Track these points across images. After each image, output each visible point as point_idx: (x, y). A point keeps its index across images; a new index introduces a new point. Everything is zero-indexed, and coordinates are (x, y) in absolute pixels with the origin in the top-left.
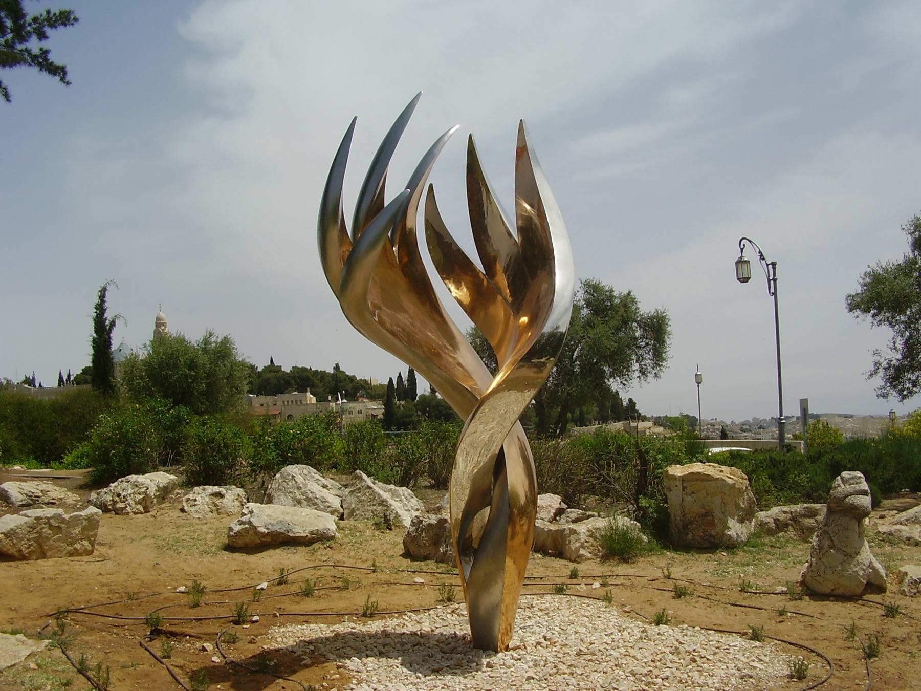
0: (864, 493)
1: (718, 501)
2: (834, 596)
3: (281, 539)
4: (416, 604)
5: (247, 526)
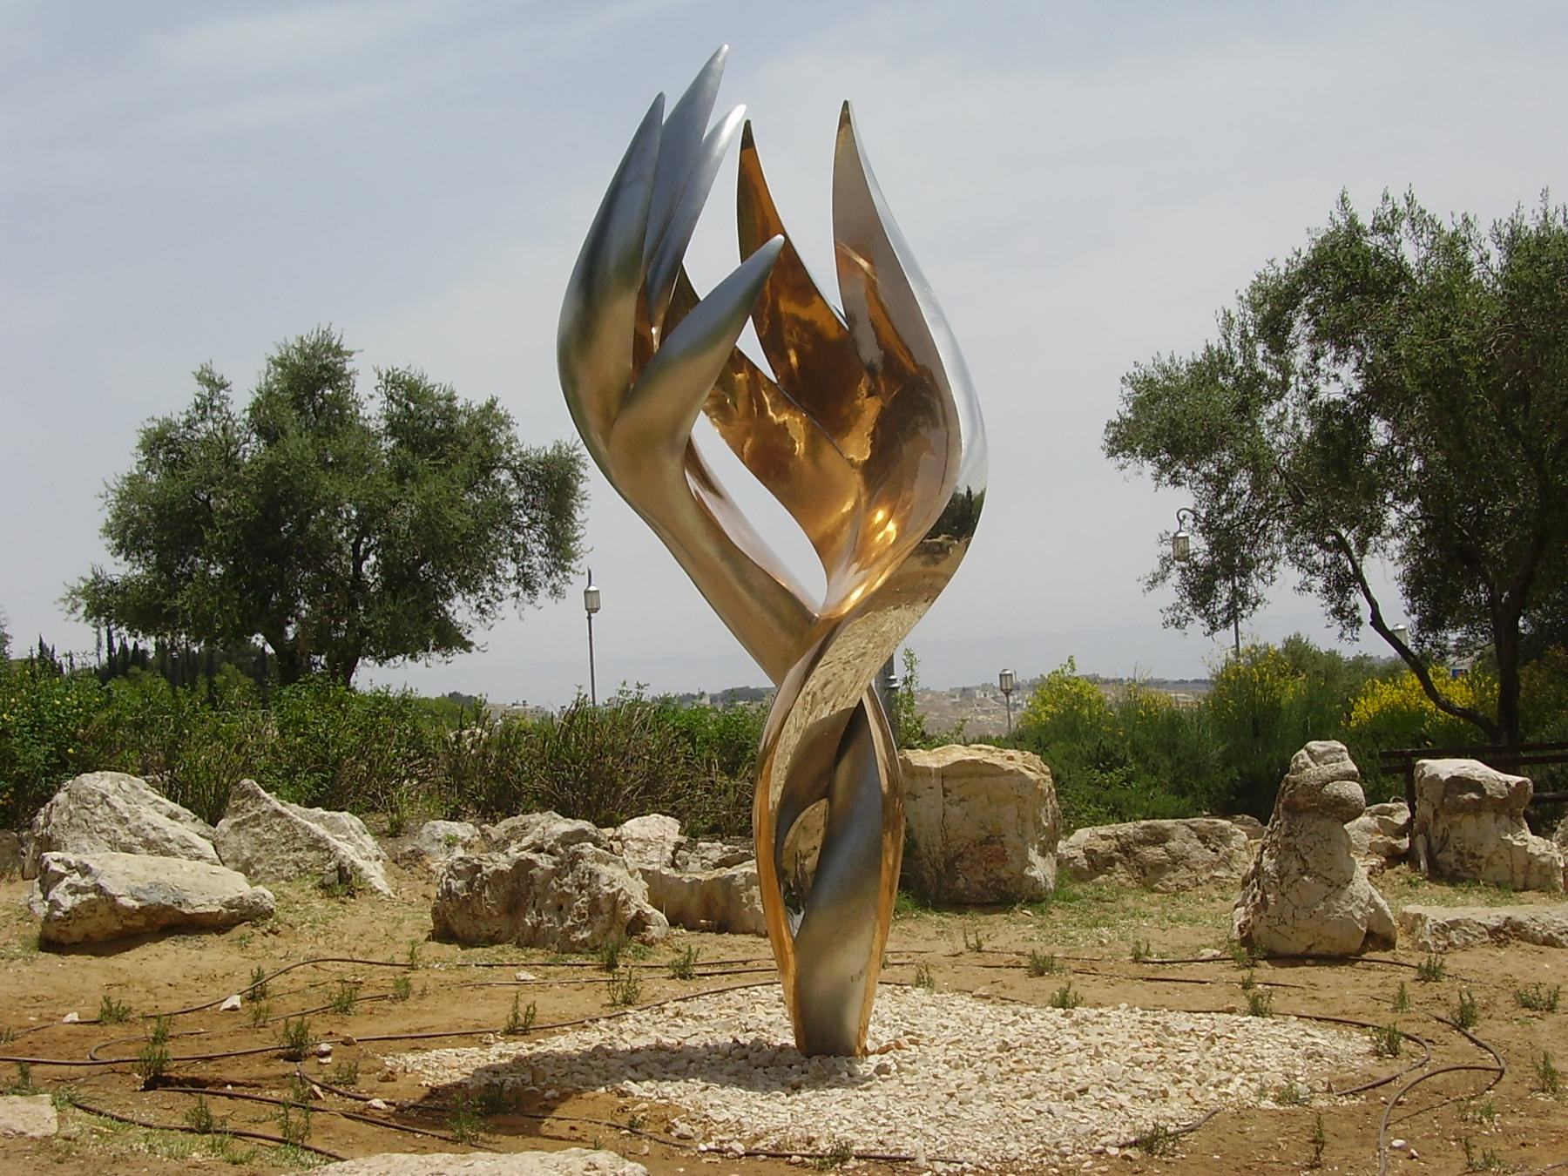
0: (1349, 777)
1: (1010, 813)
2: (1312, 957)
3: (163, 921)
4: (575, 1014)
5: (92, 895)
